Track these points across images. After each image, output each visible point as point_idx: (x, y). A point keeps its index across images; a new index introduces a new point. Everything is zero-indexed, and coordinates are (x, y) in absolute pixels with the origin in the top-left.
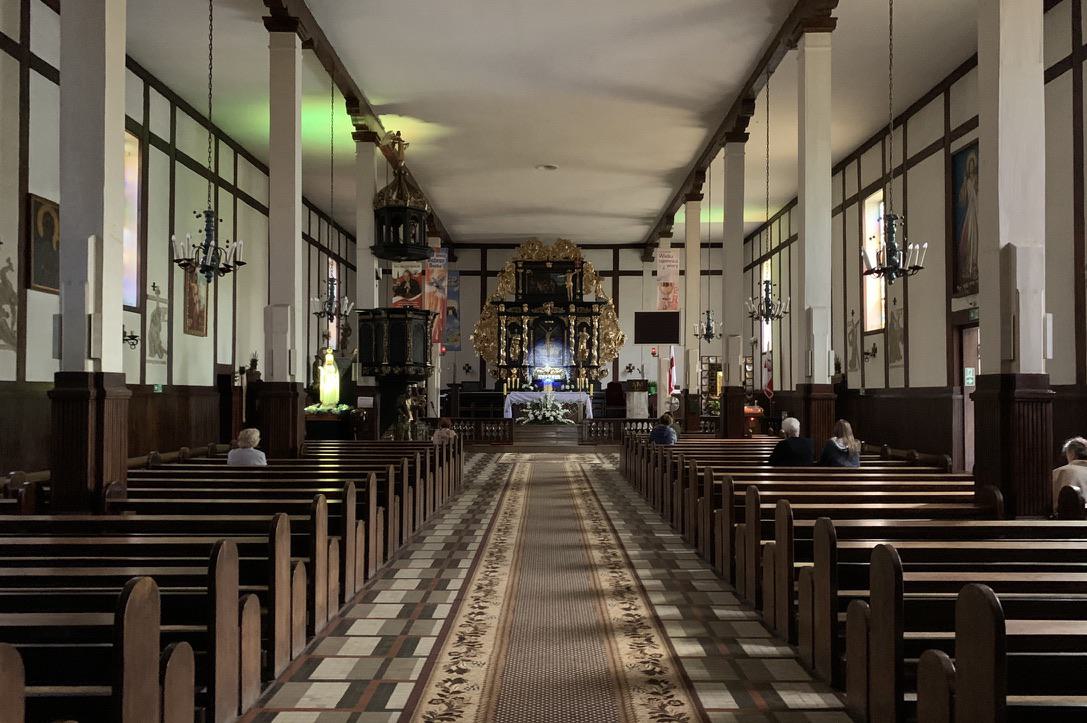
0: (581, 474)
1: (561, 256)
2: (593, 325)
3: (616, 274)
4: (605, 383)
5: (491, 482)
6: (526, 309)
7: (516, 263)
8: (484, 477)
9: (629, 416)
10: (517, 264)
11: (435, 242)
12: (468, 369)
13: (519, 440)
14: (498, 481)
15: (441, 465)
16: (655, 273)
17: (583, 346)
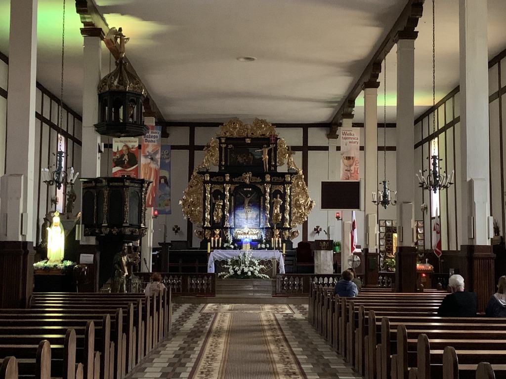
0: (275, 322)
2: (285, 193)
3: (305, 149)
4: (296, 242)
6: (228, 178)
8: (189, 325)
9: (316, 272)
11: (150, 121)
12: (177, 230)
13: (221, 292)
16: (338, 148)
17: (277, 210)
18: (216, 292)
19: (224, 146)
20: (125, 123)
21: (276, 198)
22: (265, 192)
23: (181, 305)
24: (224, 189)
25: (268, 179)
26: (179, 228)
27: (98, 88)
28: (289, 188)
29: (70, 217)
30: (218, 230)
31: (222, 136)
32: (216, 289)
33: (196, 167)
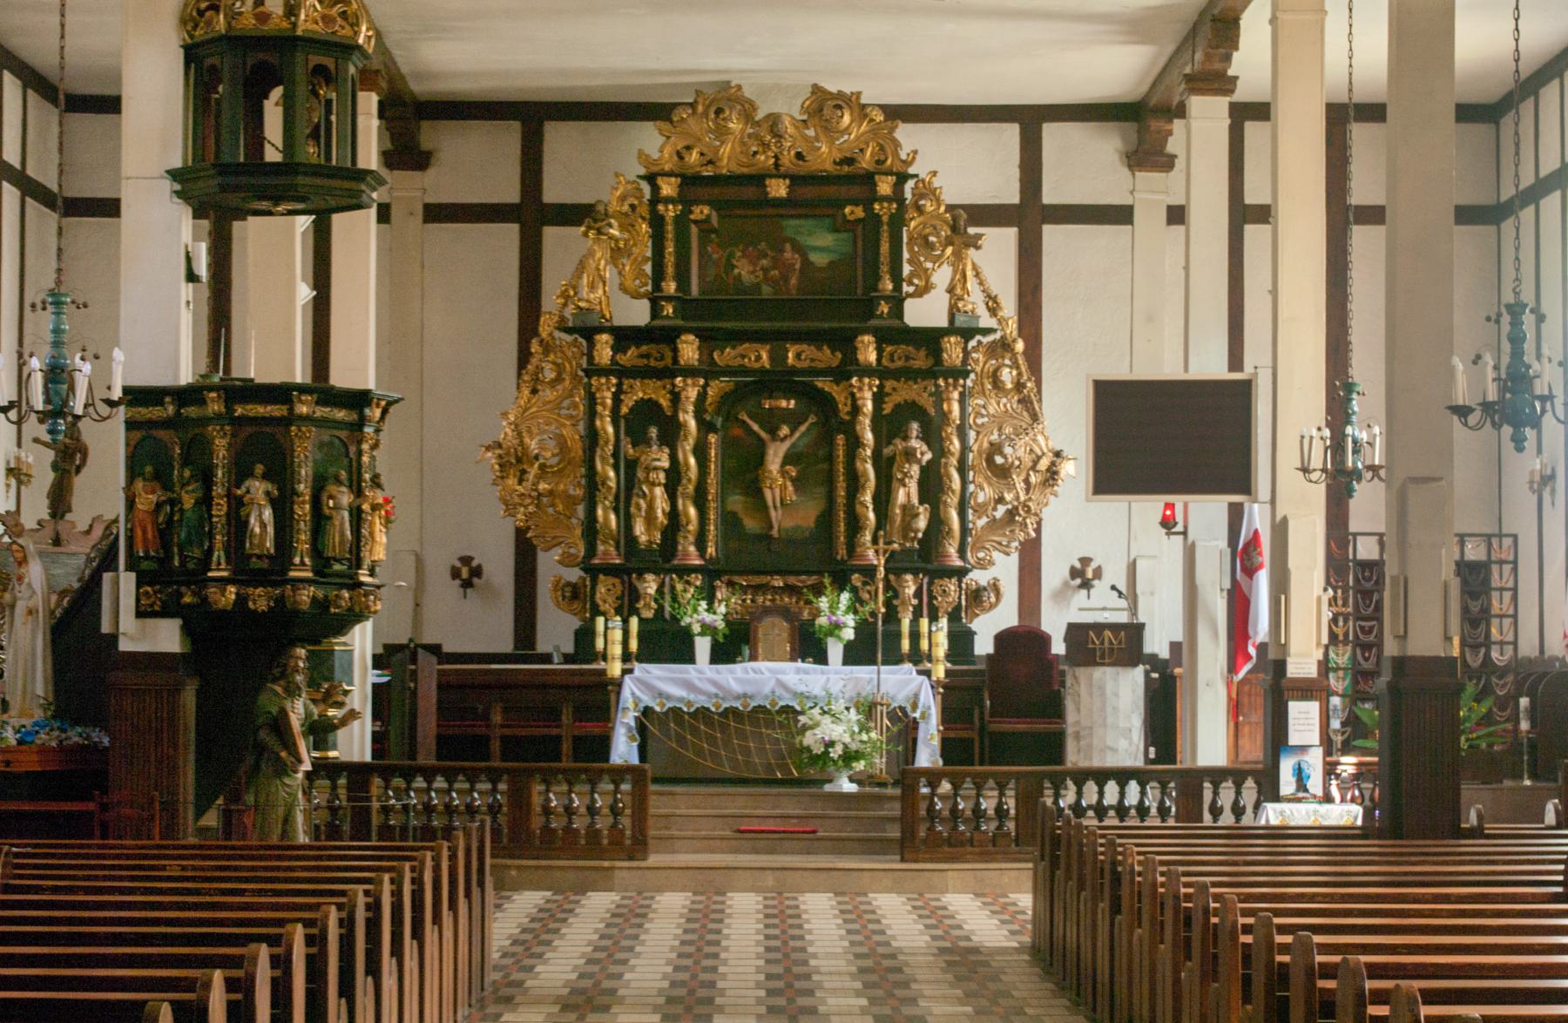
1: (824, 156)
2: (945, 417)
4: (985, 632)
5: (587, 983)
7: (651, 178)
9: (1074, 757)
10: (655, 189)
12: (468, 575)
13: (669, 844)
14: (606, 984)
15: (437, 918)
17: (907, 493)
18: (651, 842)
19: (671, 212)
20: (288, 167)
21: (906, 438)
22: (856, 410)
23: (508, 898)
24: (676, 398)
25: (870, 356)
26: (479, 567)
27: (183, 22)
28: (956, 395)
29: (64, 536)
30: (650, 577)
31: (667, 168)
32: (652, 832)
33: (550, 301)
